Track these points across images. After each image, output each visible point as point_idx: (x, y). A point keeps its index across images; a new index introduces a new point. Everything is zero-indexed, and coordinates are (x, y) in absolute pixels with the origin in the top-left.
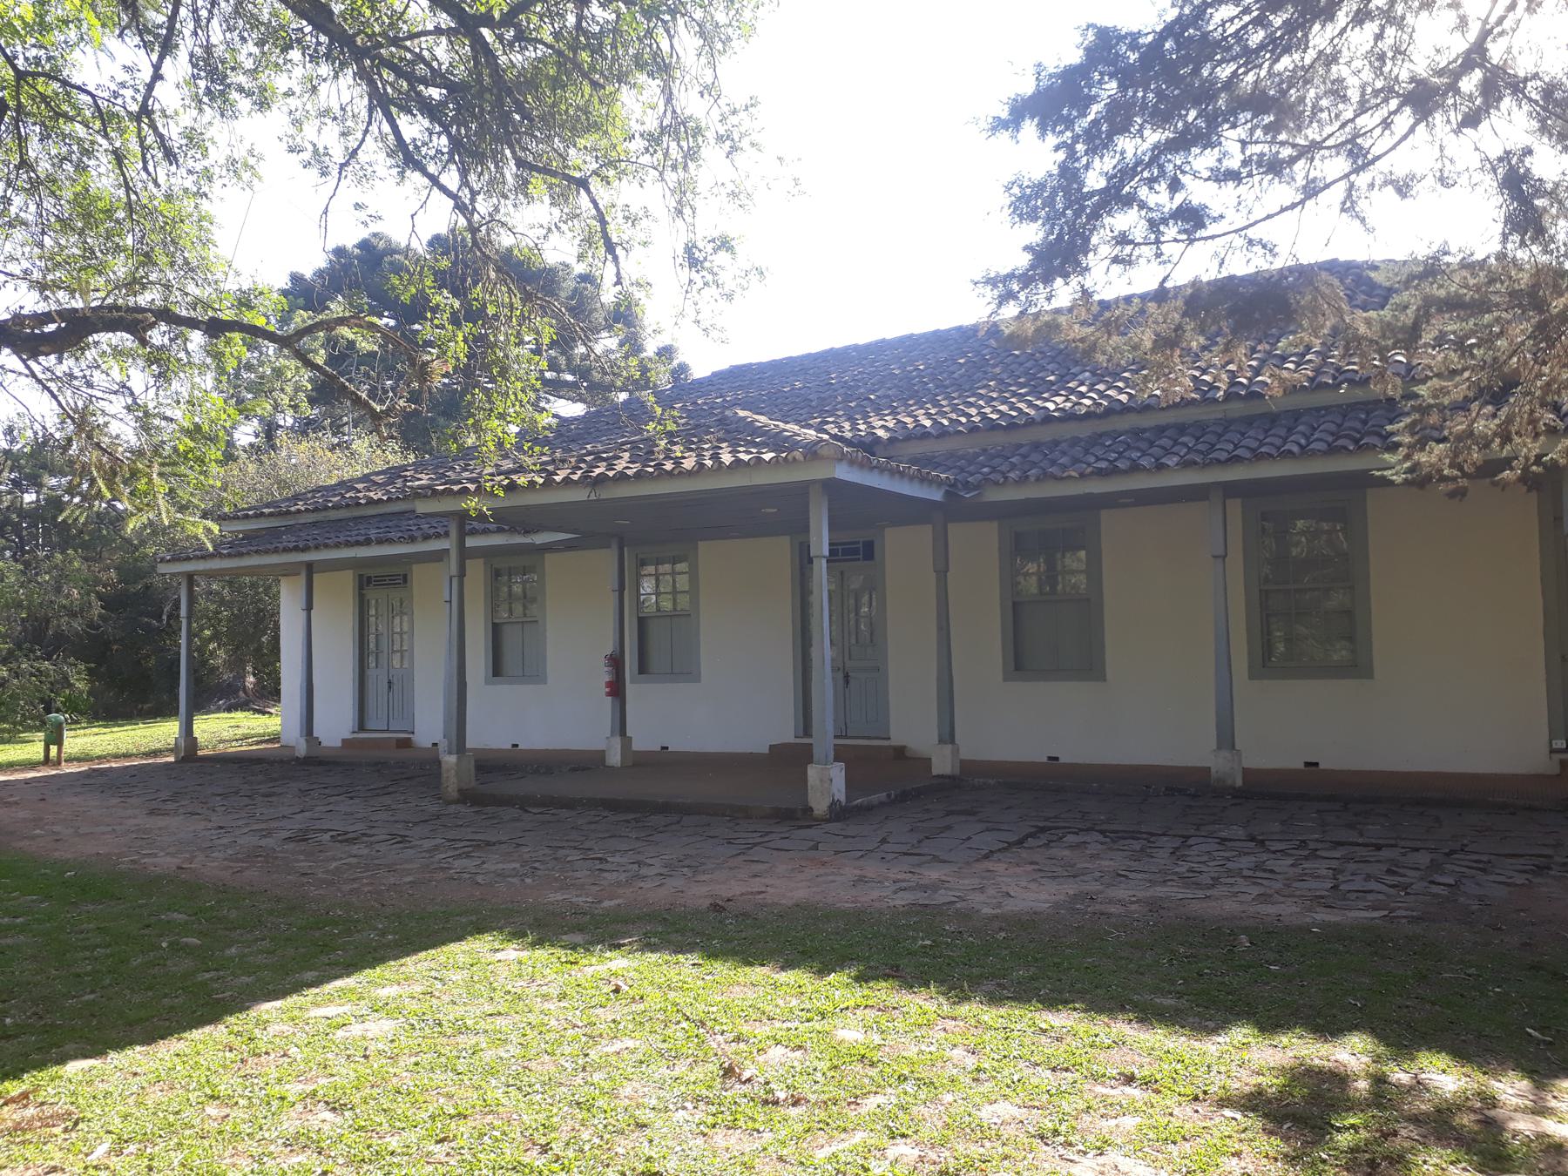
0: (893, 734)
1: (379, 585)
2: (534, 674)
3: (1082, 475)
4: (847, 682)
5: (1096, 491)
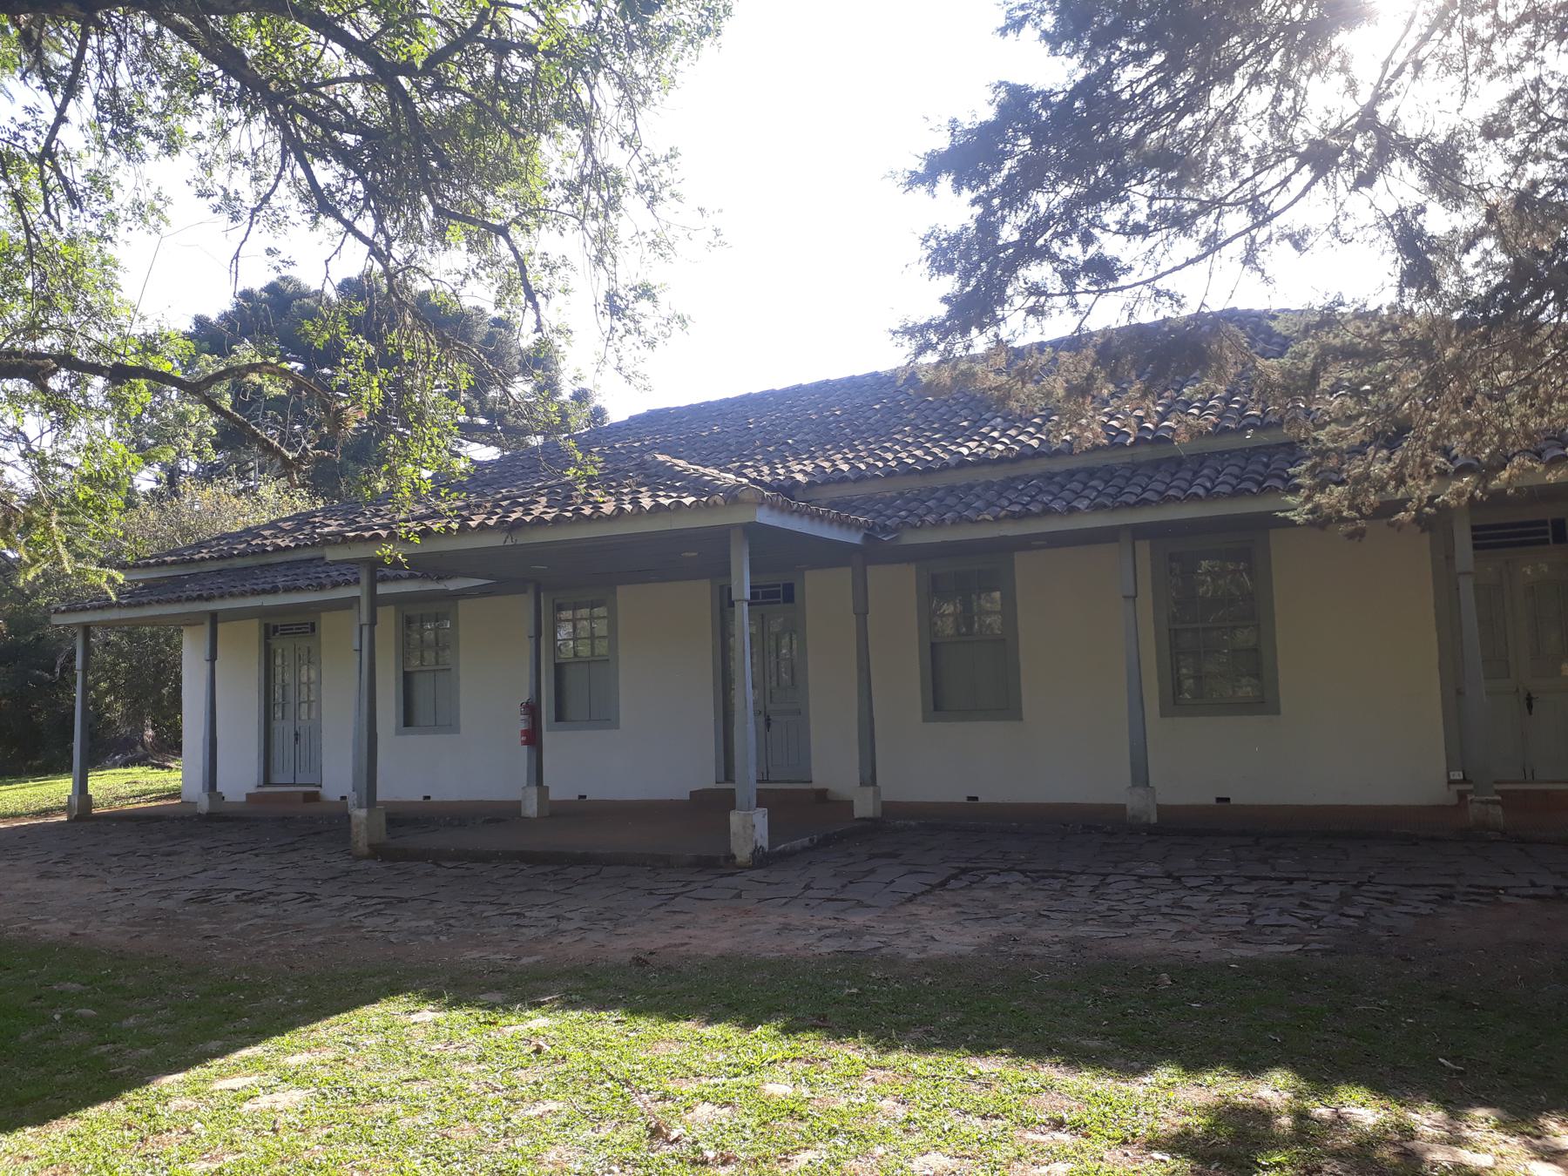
0: (814, 778)
1: (286, 635)
2: (447, 724)
3: (997, 519)
4: (1530, 706)
5: (1010, 533)
